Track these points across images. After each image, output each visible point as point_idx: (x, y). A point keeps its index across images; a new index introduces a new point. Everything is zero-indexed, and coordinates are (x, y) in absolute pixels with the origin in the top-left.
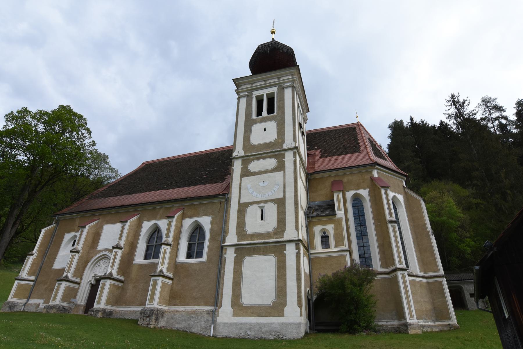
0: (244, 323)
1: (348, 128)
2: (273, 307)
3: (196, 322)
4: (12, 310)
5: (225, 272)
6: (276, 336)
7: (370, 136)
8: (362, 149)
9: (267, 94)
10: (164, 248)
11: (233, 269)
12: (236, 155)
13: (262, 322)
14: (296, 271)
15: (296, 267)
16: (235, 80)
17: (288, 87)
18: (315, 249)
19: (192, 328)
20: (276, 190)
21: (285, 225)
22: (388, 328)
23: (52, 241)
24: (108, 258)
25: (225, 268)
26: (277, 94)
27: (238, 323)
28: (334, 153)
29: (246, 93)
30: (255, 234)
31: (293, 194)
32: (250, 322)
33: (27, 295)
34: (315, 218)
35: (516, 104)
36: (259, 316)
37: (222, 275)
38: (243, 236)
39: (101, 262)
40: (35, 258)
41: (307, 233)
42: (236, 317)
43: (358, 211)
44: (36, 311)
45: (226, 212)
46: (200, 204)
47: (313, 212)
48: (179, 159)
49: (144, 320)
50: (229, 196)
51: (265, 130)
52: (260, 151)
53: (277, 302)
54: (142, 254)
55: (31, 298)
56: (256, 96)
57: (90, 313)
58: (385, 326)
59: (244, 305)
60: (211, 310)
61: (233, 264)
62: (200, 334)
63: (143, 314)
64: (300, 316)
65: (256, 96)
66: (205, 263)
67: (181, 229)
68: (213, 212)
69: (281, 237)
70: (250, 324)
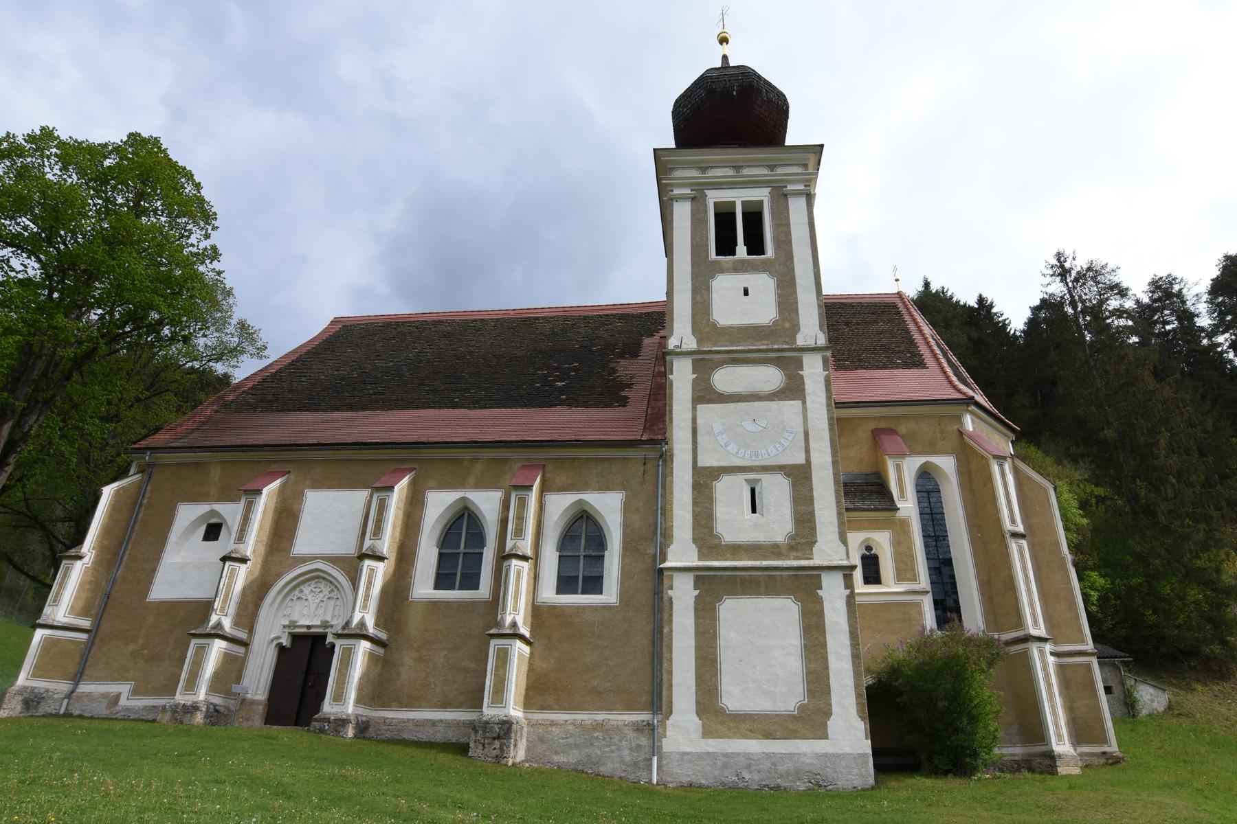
0: (733, 753)
4: (34, 711)
5: (672, 631)
9: (743, 202)
11: (693, 625)
13: (775, 751)
15: (848, 629)
16: (658, 152)
19: (597, 763)
20: (786, 444)
21: (814, 529)
23: (135, 522)
24: (324, 579)
26: (771, 206)
28: (865, 362)
29: (687, 191)
30: (743, 545)
33: (73, 668)
35: (1149, 284)
36: (767, 738)
38: (711, 547)
39: (306, 589)
40: (89, 566)
44: (112, 713)
46: (588, 459)
49: (486, 745)
51: (746, 293)
53: (810, 706)
54: (431, 573)
55: (84, 677)
57: (318, 727)
60: (643, 721)
63: (480, 732)
66: (617, 607)
70: (748, 756)
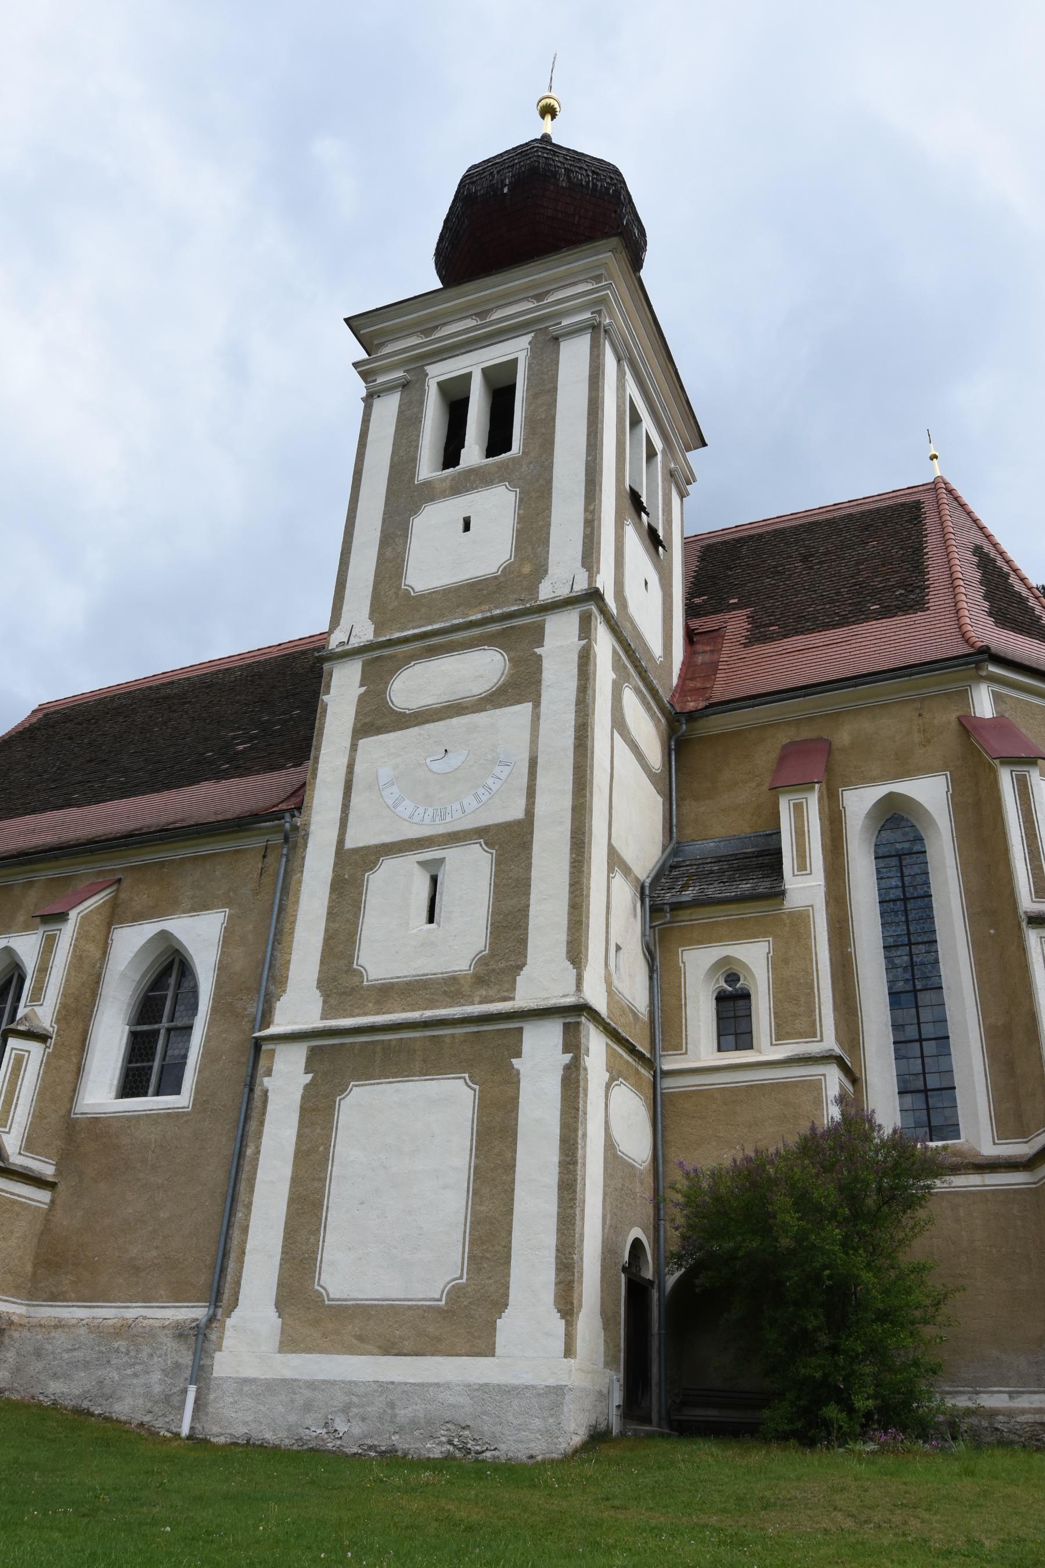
0: (324, 1382)
1: (888, 507)
2: (447, 1312)
3: (129, 1372)
6: (455, 1446)
7: (988, 537)
8: (937, 597)
9: (485, 371)
10: (12, 1049)
12: (342, 643)
13: (397, 1379)
14: (560, 1148)
15: (558, 1132)
17: (575, 331)
18: (686, 1053)
20: (494, 788)
21: (523, 942)
22: (1018, 1427)
25: (260, 1138)
27: (301, 1380)
30: (397, 983)
31: (567, 802)
32: (348, 1379)
34: (689, 911)
36: (386, 1352)
37: (247, 1168)
38: (344, 993)
41: (651, 978)
42: (294, 1352)
43: (902, 877)
45: (285, 890)
47: (685, 887)
48: (172, 683)
50: (299, 822)
51: (467, 527)
52: (441, 617)
56: (438, 383)
58: (1003, 1415)
59: (327, 1302)
61: (295, 1117)
62: (142, 1424)
64: (565, 1357)
65: (438, 383)
67: (101, 968)
68: (231, 894)
69: (506, 994)
70: (350, 1387)
